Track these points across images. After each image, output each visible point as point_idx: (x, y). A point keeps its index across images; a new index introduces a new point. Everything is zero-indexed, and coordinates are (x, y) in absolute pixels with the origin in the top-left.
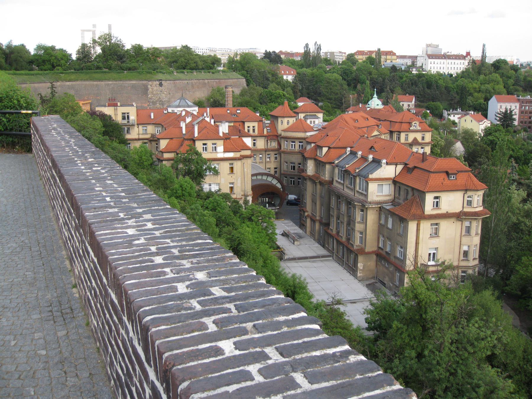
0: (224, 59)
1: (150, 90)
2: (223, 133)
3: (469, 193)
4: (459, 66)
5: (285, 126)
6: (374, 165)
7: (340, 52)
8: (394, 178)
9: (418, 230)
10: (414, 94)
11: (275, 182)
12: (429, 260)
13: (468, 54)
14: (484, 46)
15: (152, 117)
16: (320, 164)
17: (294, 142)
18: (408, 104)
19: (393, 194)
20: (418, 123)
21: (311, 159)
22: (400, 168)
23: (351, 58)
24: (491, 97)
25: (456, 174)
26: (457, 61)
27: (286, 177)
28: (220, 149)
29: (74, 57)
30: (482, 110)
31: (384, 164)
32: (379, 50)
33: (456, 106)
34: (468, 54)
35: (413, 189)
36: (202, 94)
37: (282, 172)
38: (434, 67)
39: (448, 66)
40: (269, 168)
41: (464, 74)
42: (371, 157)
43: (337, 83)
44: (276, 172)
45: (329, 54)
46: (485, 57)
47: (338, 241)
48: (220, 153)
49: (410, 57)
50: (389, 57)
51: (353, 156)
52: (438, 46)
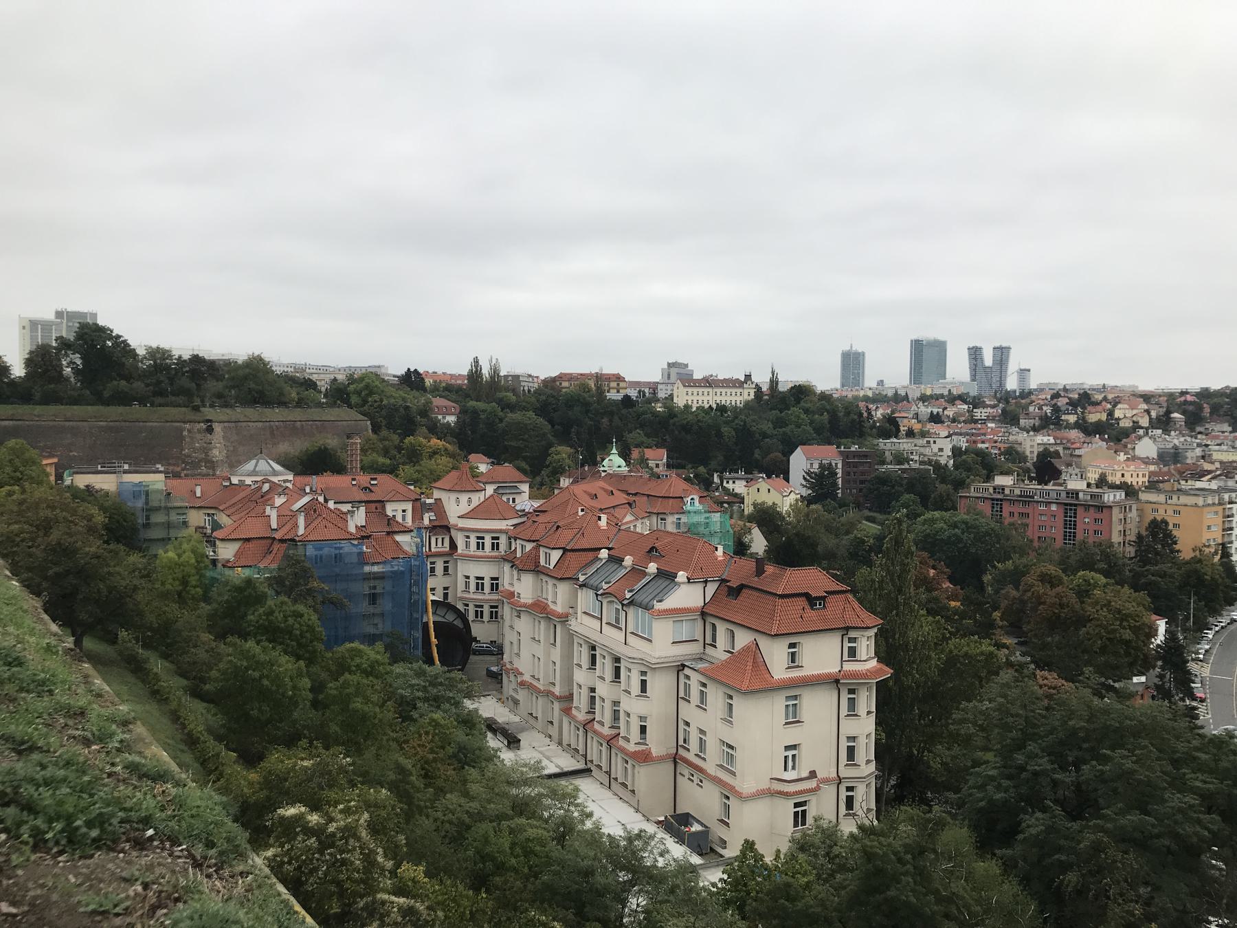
0: (323, 386)
3: (852, 634)
6: (663, 583)
13: (748, 377)
15: (198, 494)
18: (658, 458)
20: (696, 498)
22: (711, 589)
23: (550, 383)
25: (823, 598)
29: (18, 371)
30: (780, 470)
34: (748, 377)
36: (295, 447)
42: (652, 568)
46: (777, 383)
51: (613, 566)
52: (687, 365)
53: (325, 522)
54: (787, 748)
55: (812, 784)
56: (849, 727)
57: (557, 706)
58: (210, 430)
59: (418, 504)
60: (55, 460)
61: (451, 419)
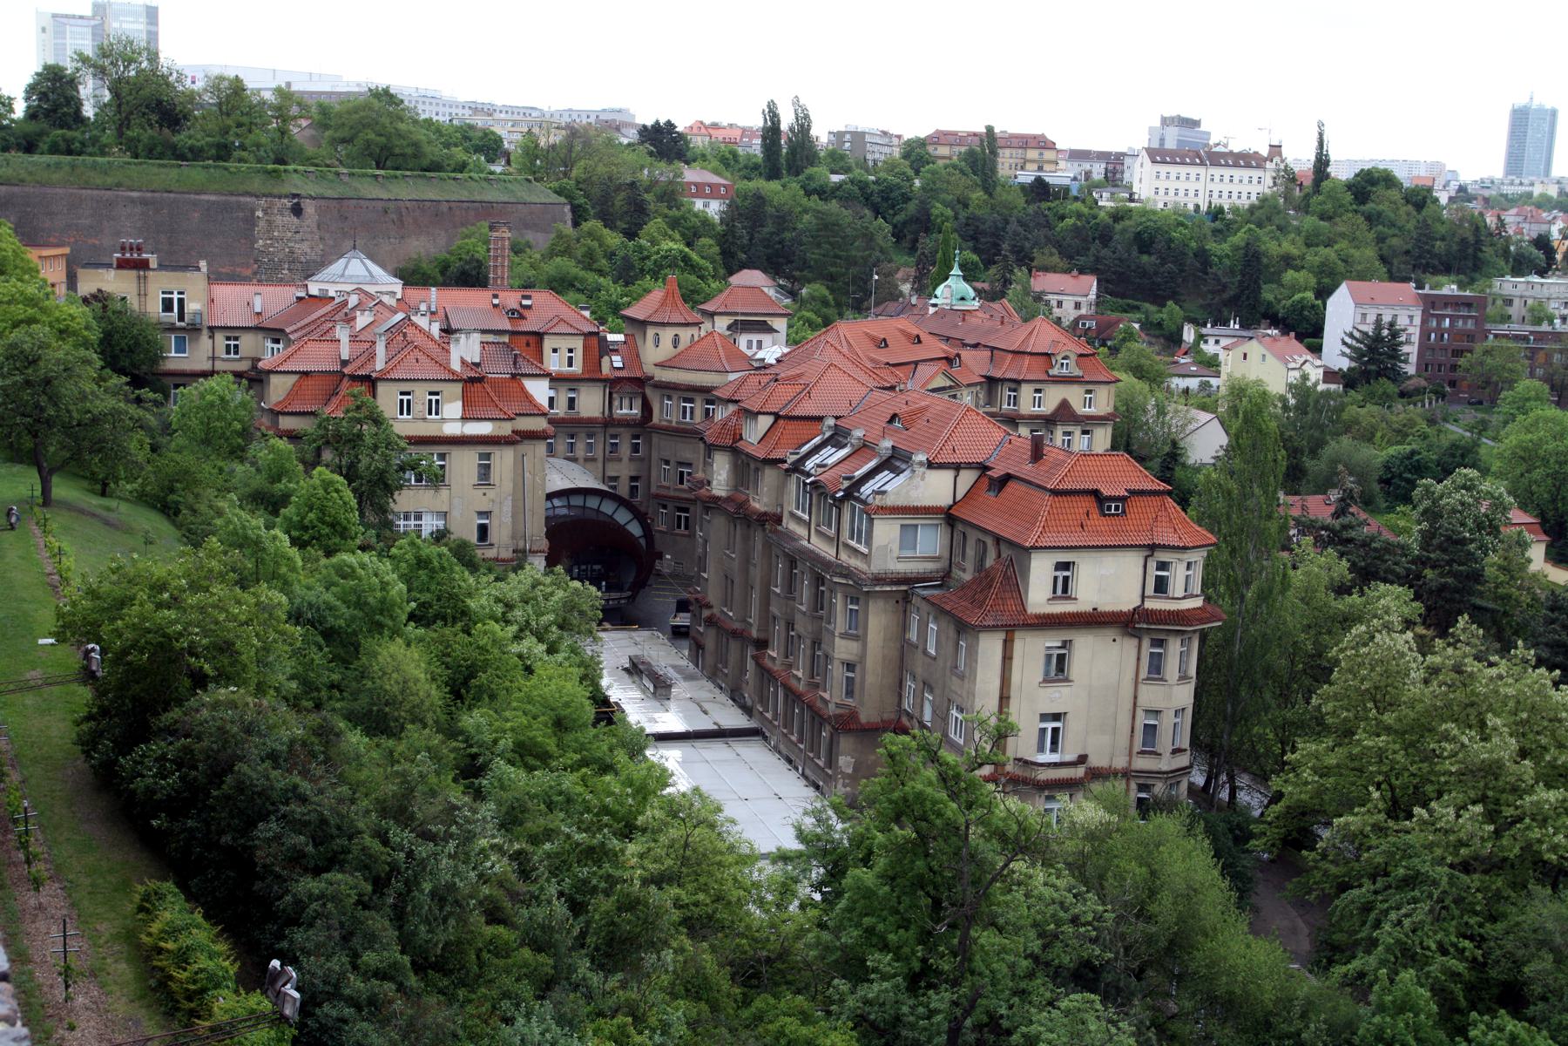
1: (262, 224)
2: (463, 362)
4: (1245, 189)
5: (666, 350)
7: (885, 133)
8: (950, 507)
9: (1007, 658)
10: (1094, 271)
11: (622, 517)
12: (1041, 749)
13: (1276, 149)
14: (1321, 125)
16: (747, 466)
17: (691, 401)
19: (946, 554)
21: (722, 448)
22: (967, 478)
23: (916, 153)
24: (1336, 286)
25: (1122, 499)
26: (1238, 173)
27: (665, 507)
28: (453, 409)
31: (921, 464)
32: (990, 129)
33: (1225, 312)
34: (1276, 149)
35: (998, 540)
36: (424, 247)
37: (654, 490)
38: (1157, 189)
39: (1210, 186)
40: (615, 479)
41: (1262, 213)
43: (843, 225)
44: (633, 490)
45: (848, 137)
46: (1327, 163)
47: (789, 690)
48: (452, 419)
49: (1103, 156)
50: (1032, 154)
53: (417, 353)
54: (1044, 717)
55: (1080, 772)
56: (1151, 695)
57: (750, 651)
58: (297, 211)
59: (594, 340)
60: (67, 250)
61: (714, 209)
